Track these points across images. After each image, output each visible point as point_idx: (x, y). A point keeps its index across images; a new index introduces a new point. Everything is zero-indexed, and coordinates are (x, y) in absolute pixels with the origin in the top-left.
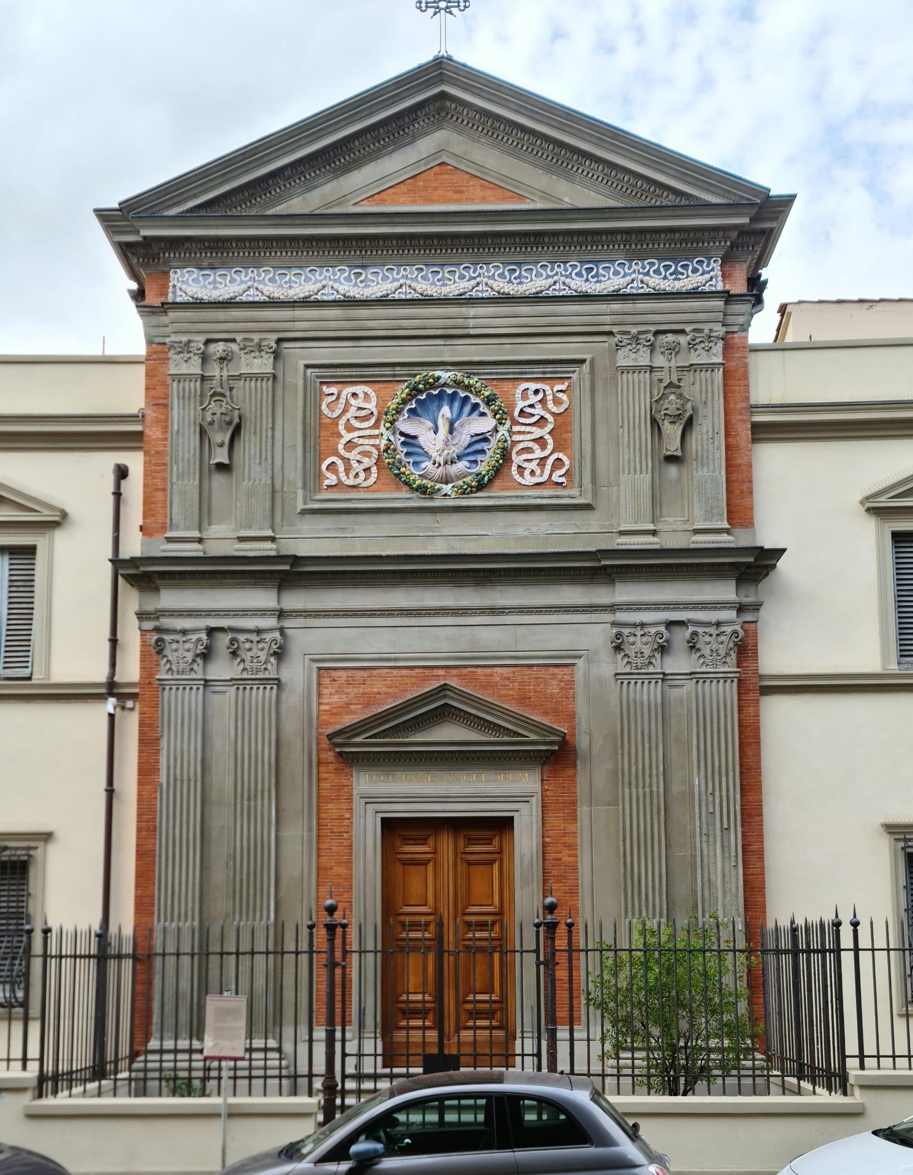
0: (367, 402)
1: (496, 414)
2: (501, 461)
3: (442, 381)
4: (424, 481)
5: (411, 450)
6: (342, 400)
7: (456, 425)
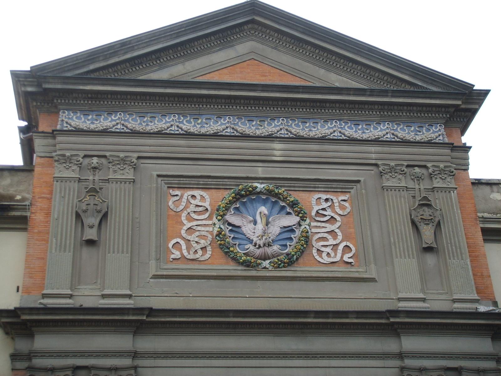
1: (299, 213)
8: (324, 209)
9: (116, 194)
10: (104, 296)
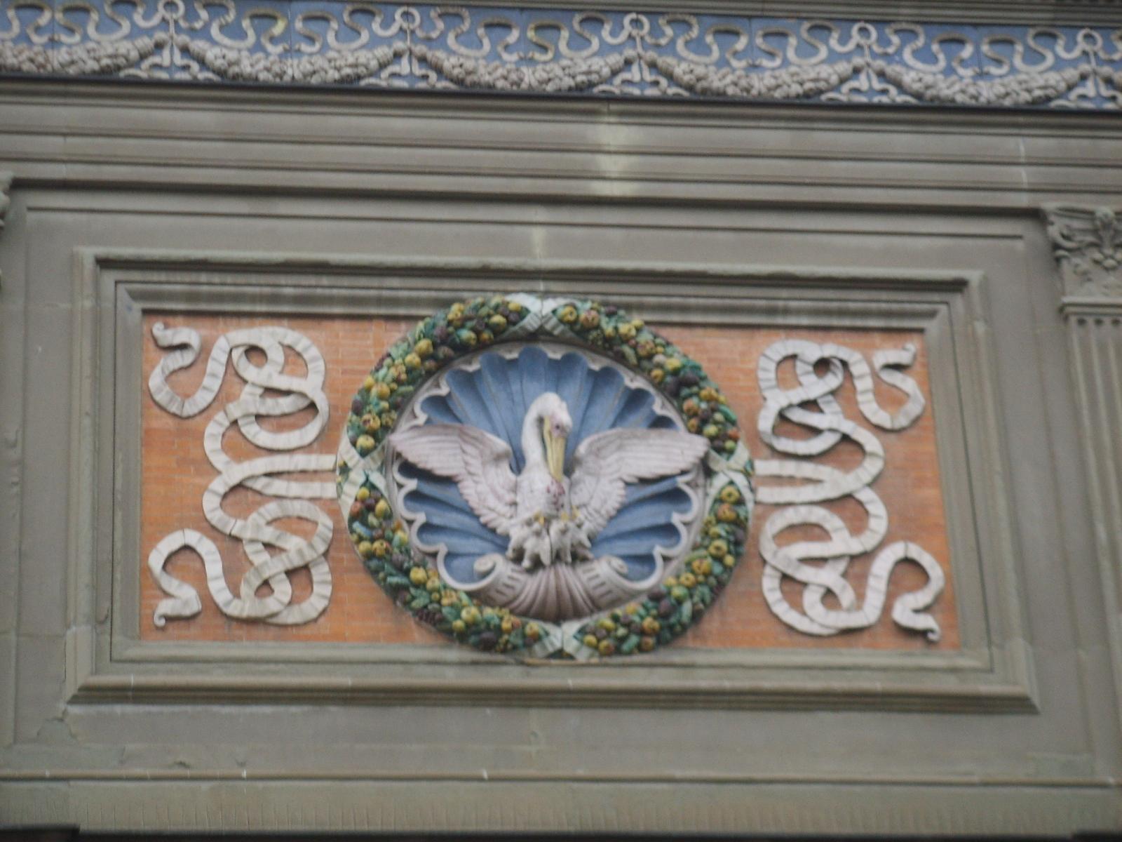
0: (293, 374)
1: (705, 421)
2: (729, 560)
3: (530, 323)
4: (489, 612)
5: (441, 518)
6: (216, 365)
7: (582, 449)
8: (810, 405)
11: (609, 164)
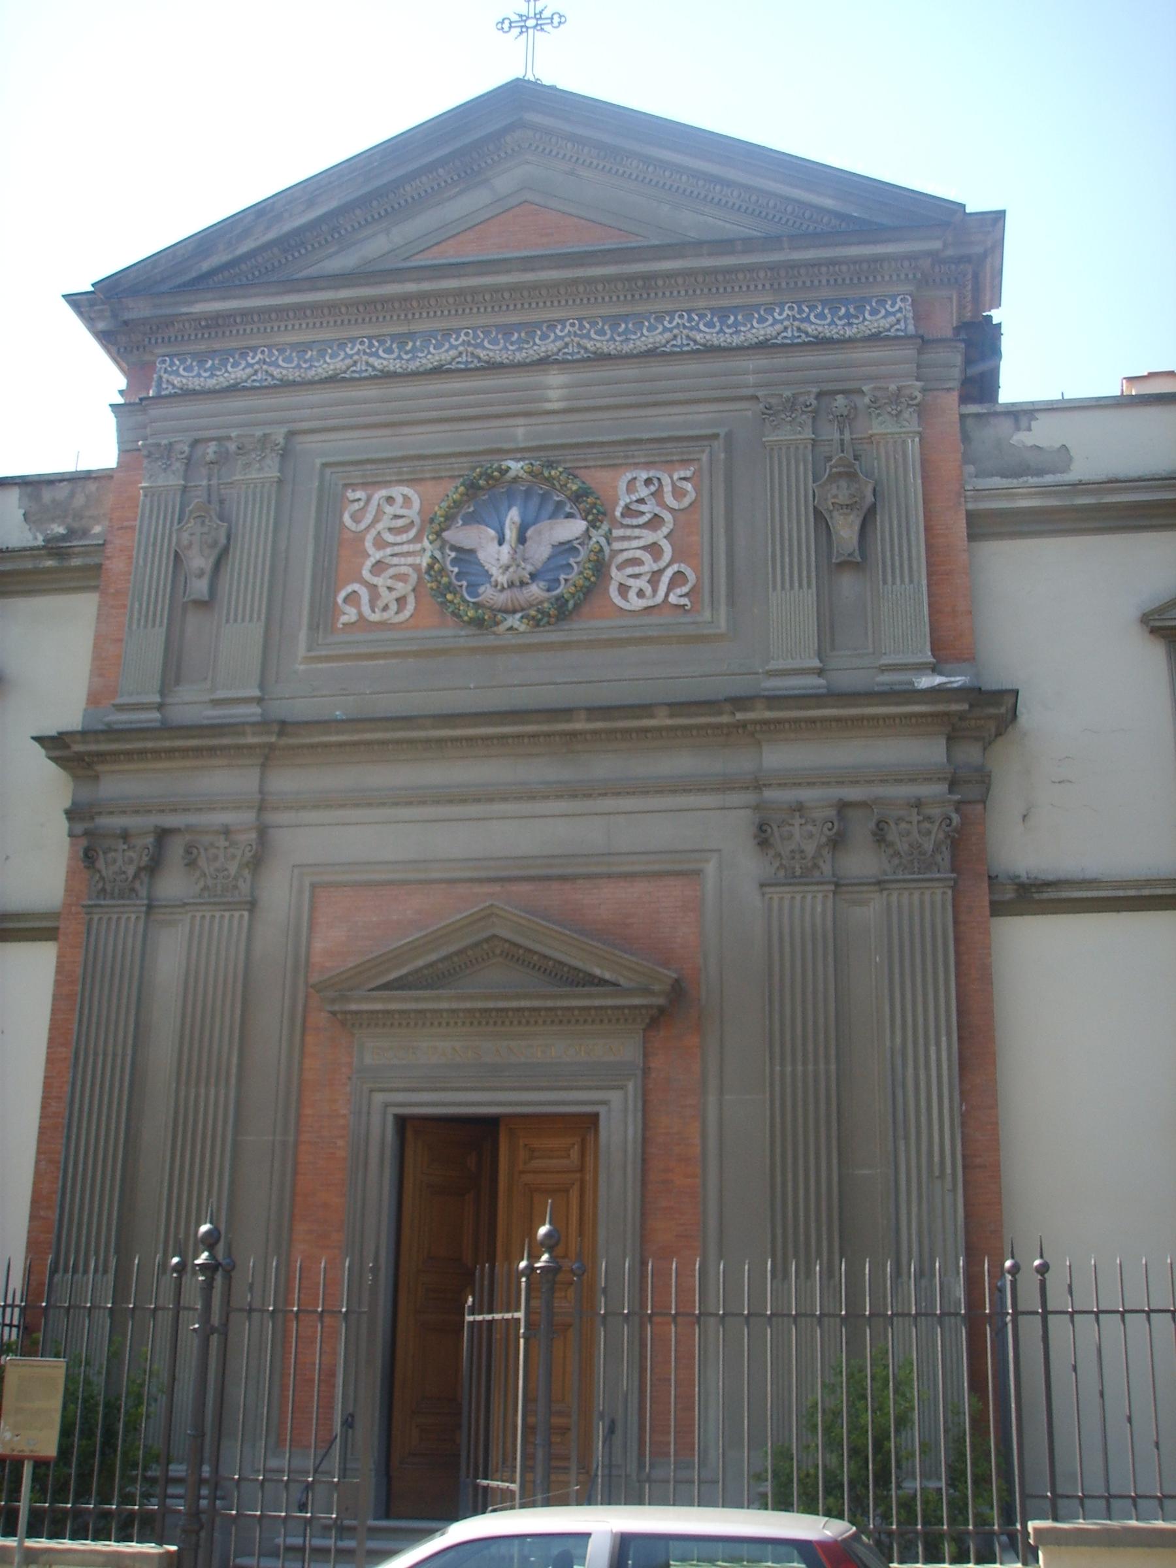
1: (588, 514)
3: (512, 474)
7: (529, 533)
8: (641, 501)
9: (246, 508)
10: (216, 703)
11: (552, 394)
